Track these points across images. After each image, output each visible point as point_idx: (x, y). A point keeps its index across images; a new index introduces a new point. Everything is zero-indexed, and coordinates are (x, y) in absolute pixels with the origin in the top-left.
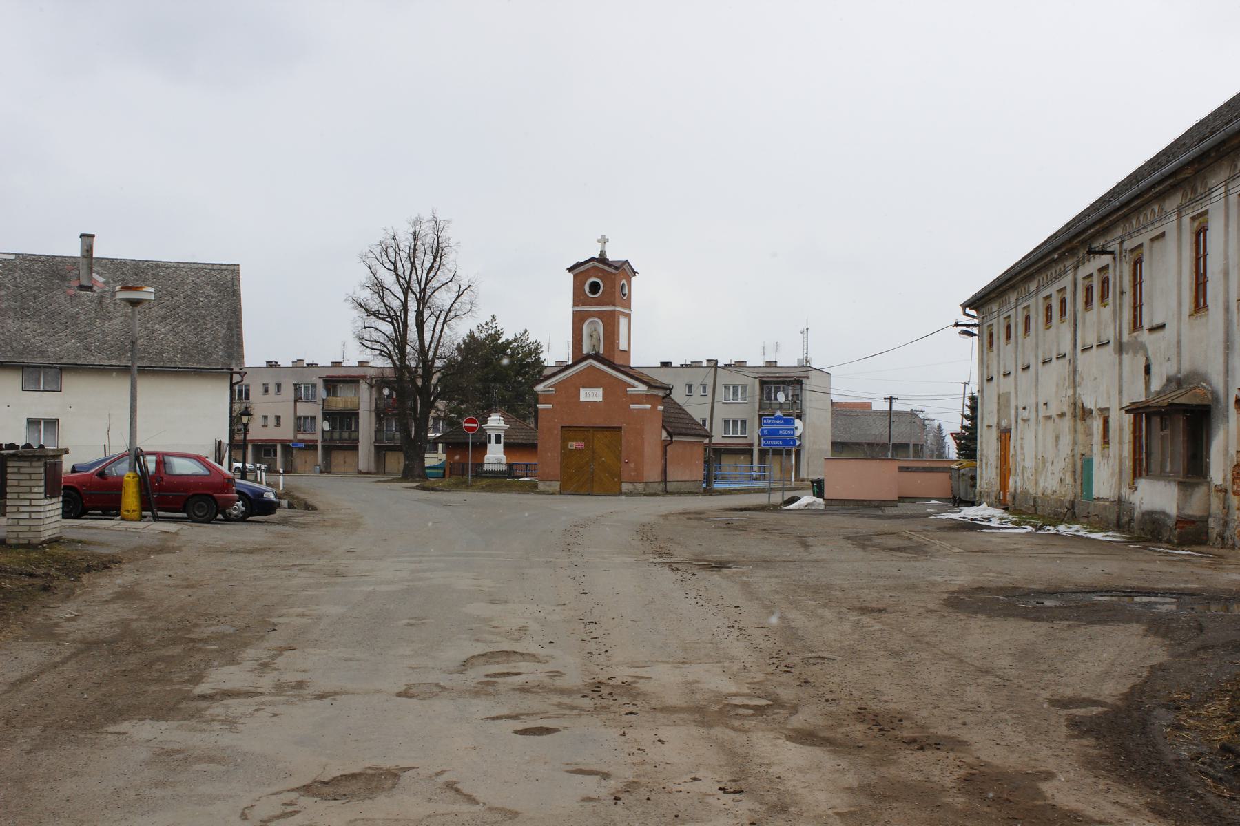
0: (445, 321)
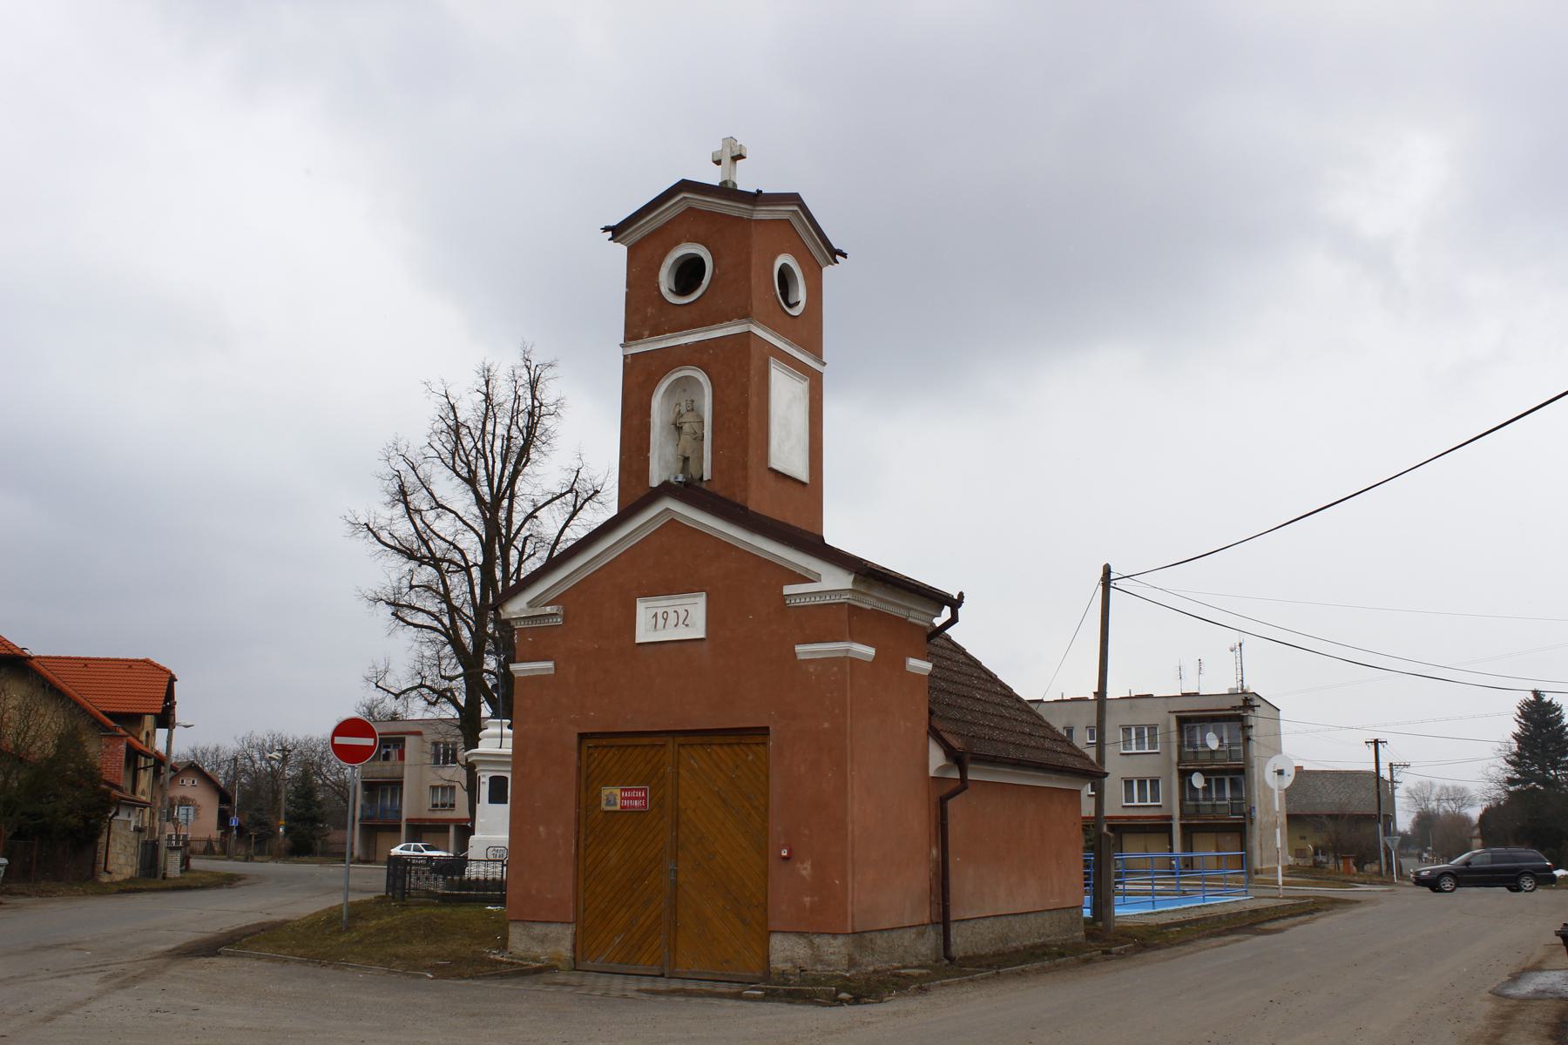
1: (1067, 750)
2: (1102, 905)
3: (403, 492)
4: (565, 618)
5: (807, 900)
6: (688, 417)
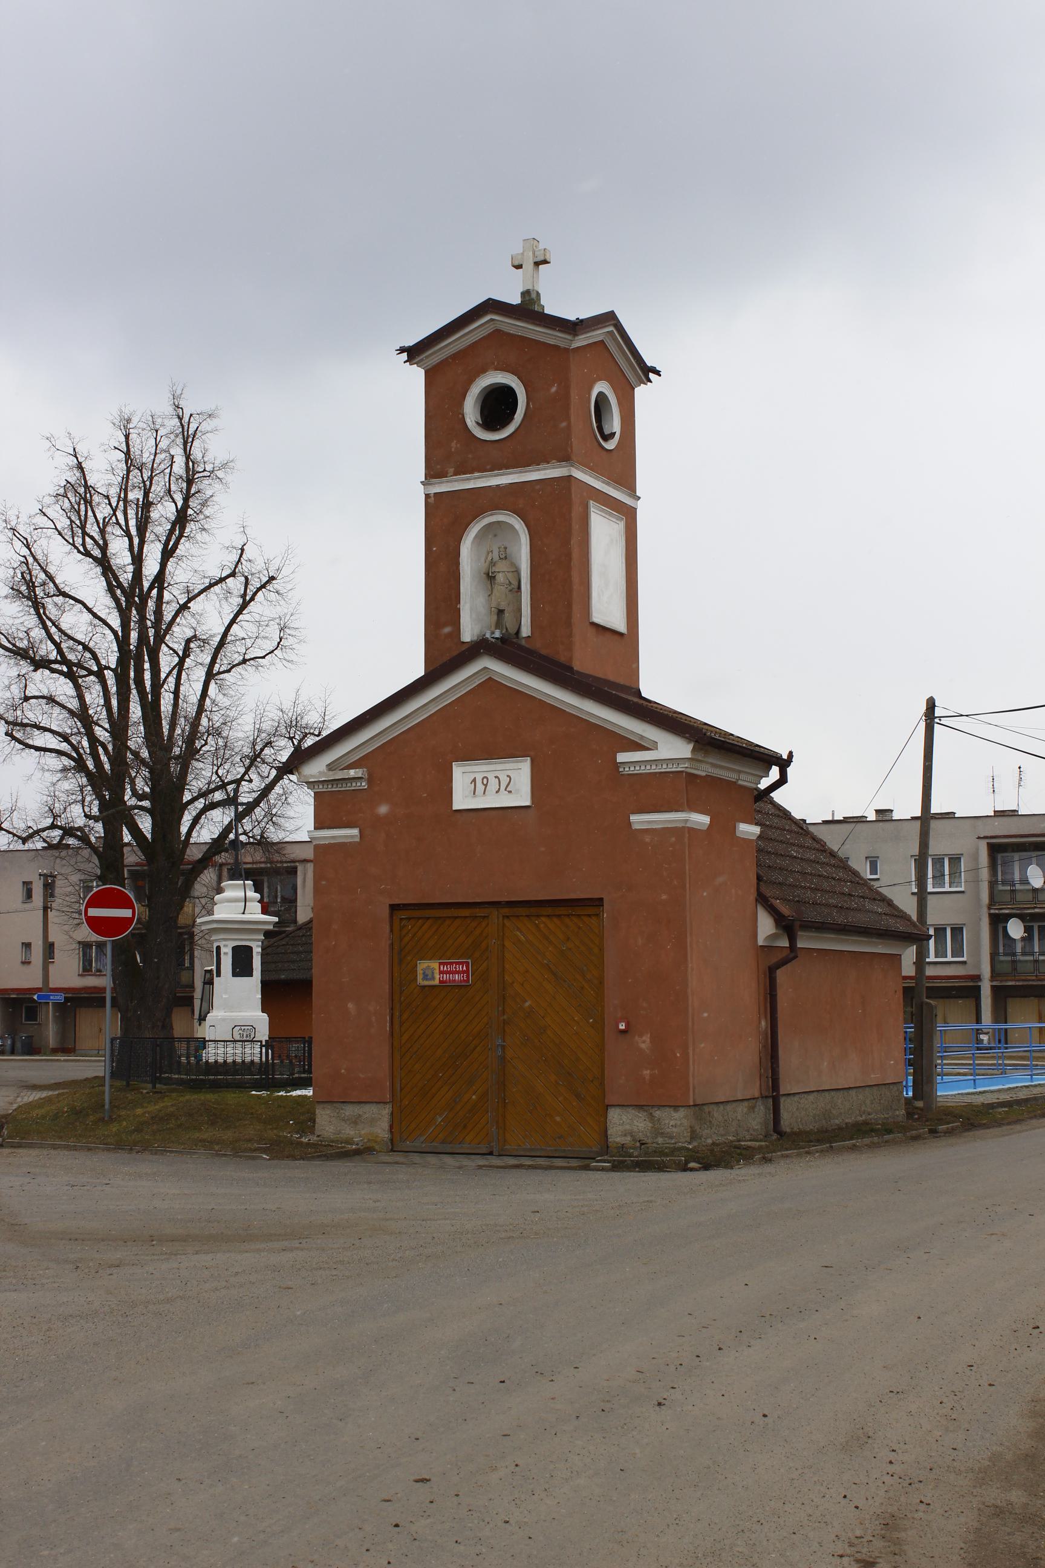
0: (210, 676)
1: (887, 910)
2: (924, 1082)
3: (31, 585)
4: (370, 780)
5: (647, 1072)
6: (501, 566)
